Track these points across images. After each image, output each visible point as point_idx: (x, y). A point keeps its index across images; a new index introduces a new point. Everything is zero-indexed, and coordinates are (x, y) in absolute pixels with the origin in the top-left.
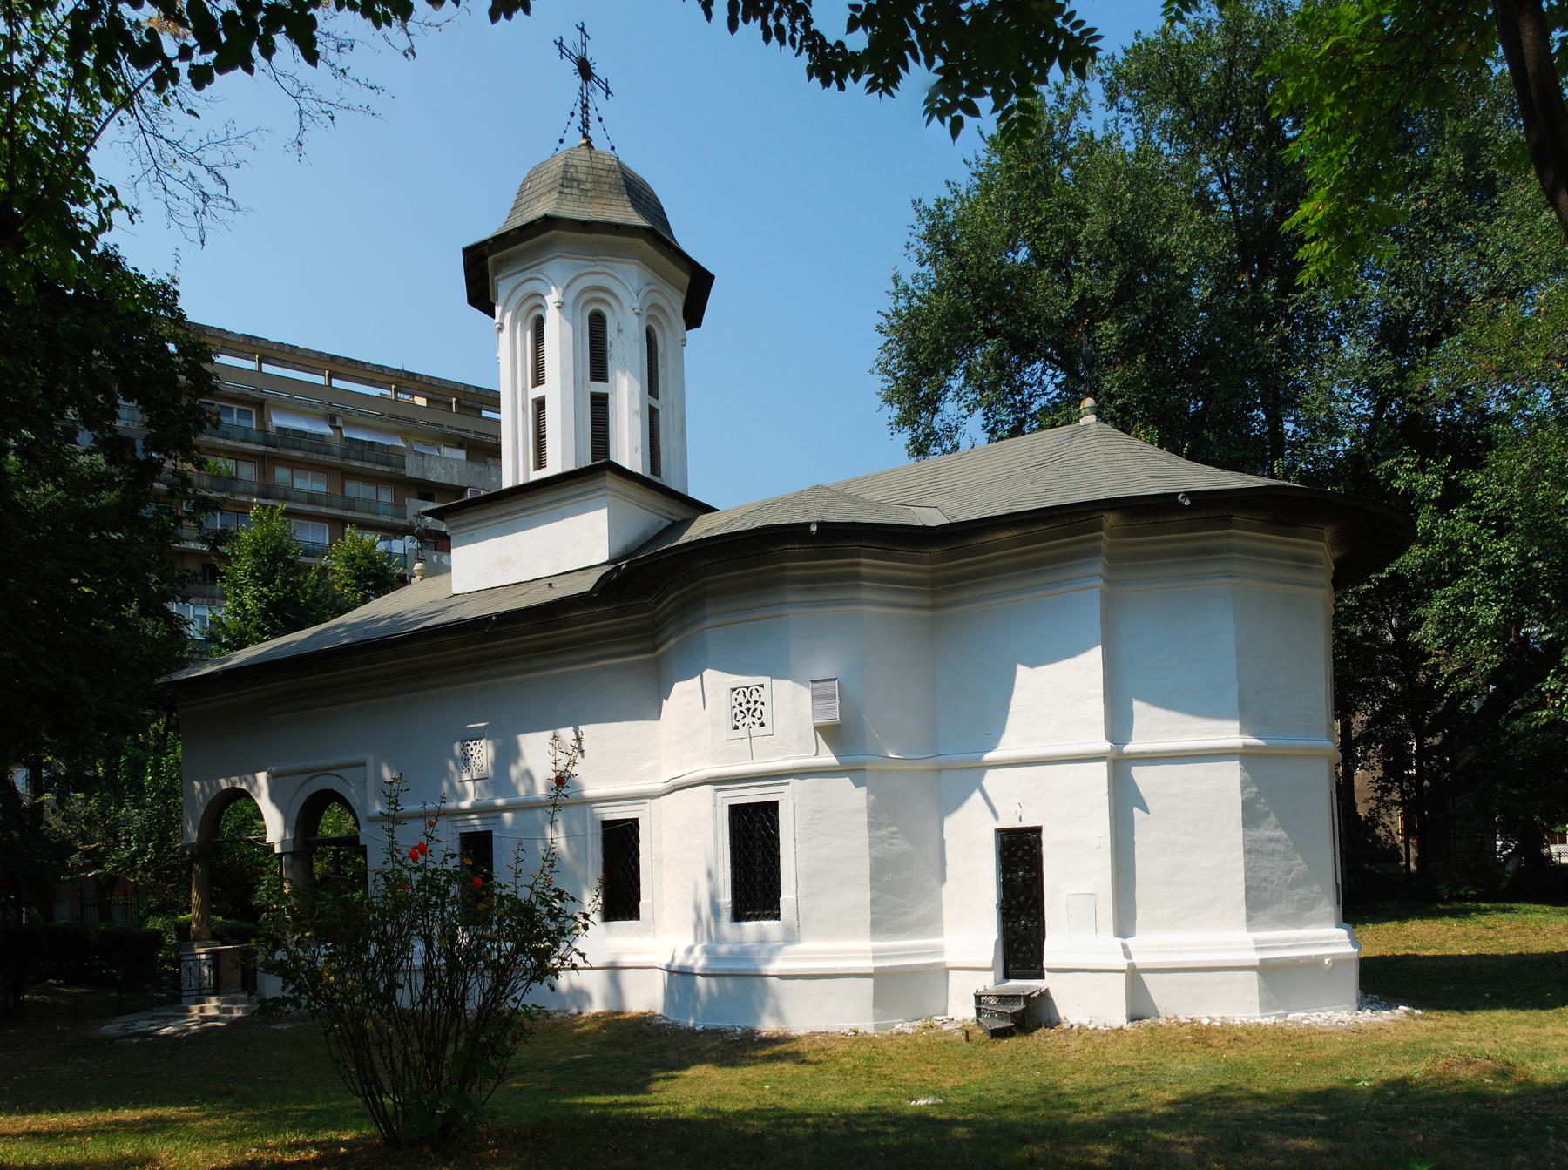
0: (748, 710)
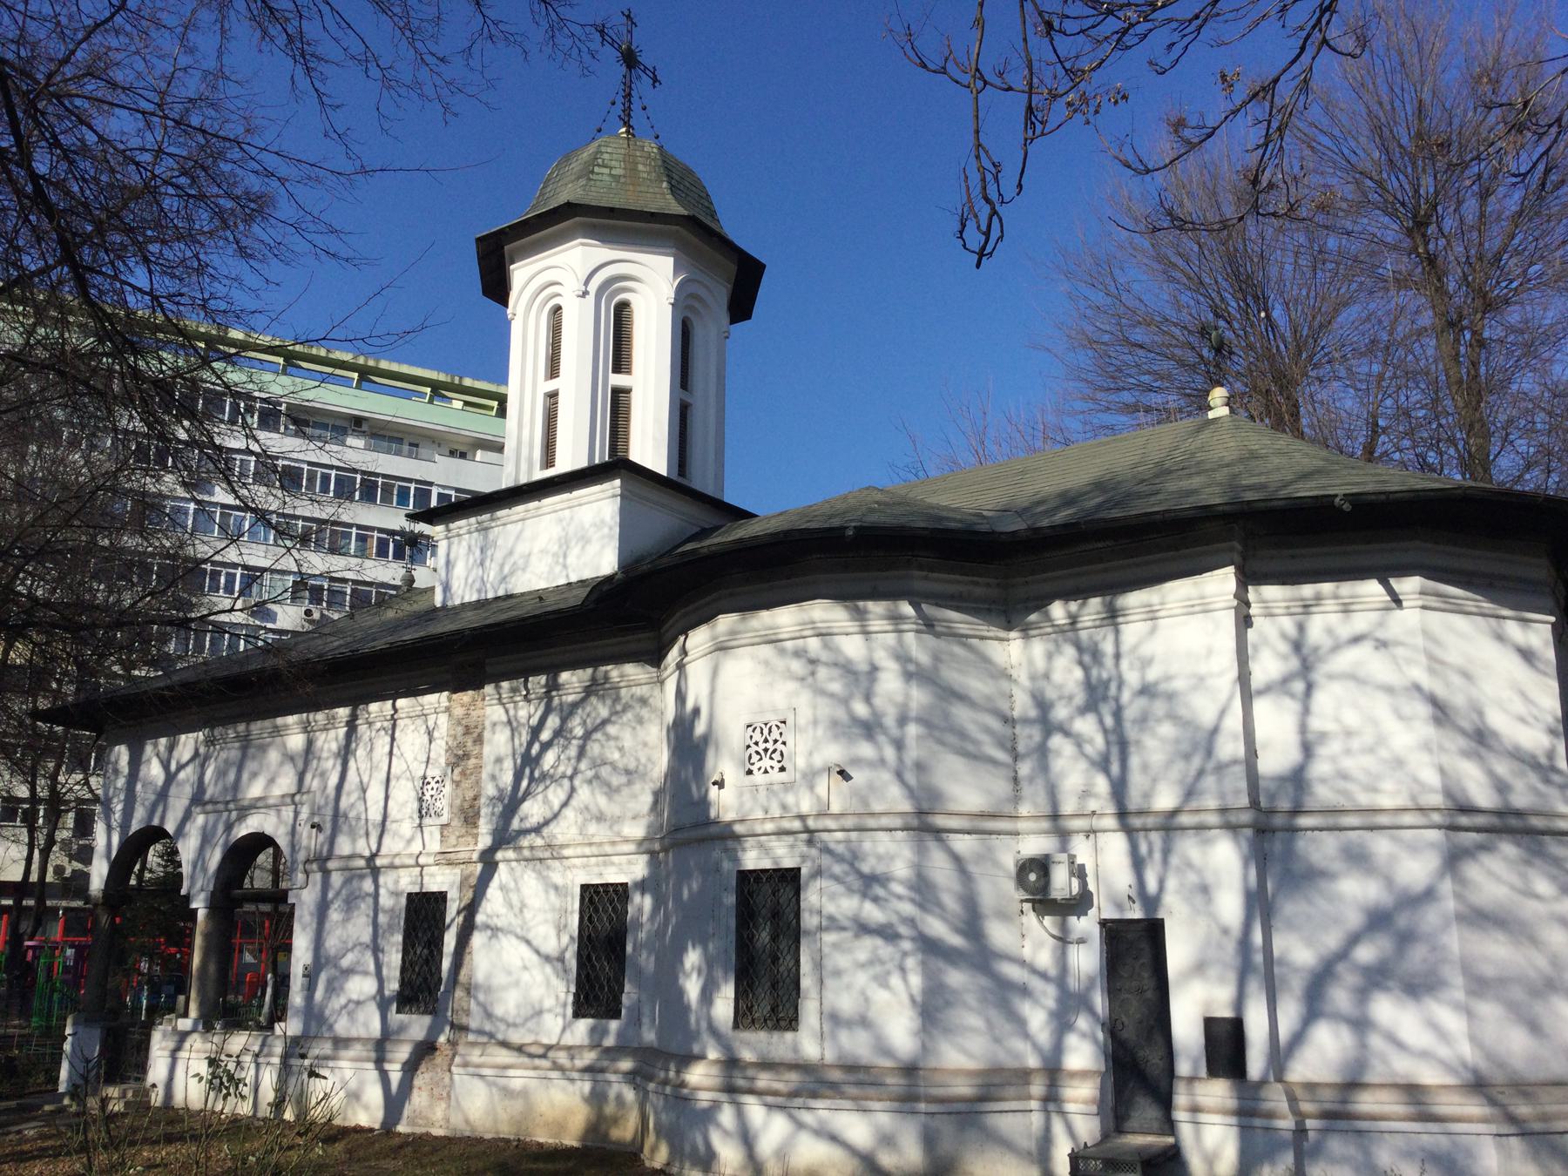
0: (766, 750)
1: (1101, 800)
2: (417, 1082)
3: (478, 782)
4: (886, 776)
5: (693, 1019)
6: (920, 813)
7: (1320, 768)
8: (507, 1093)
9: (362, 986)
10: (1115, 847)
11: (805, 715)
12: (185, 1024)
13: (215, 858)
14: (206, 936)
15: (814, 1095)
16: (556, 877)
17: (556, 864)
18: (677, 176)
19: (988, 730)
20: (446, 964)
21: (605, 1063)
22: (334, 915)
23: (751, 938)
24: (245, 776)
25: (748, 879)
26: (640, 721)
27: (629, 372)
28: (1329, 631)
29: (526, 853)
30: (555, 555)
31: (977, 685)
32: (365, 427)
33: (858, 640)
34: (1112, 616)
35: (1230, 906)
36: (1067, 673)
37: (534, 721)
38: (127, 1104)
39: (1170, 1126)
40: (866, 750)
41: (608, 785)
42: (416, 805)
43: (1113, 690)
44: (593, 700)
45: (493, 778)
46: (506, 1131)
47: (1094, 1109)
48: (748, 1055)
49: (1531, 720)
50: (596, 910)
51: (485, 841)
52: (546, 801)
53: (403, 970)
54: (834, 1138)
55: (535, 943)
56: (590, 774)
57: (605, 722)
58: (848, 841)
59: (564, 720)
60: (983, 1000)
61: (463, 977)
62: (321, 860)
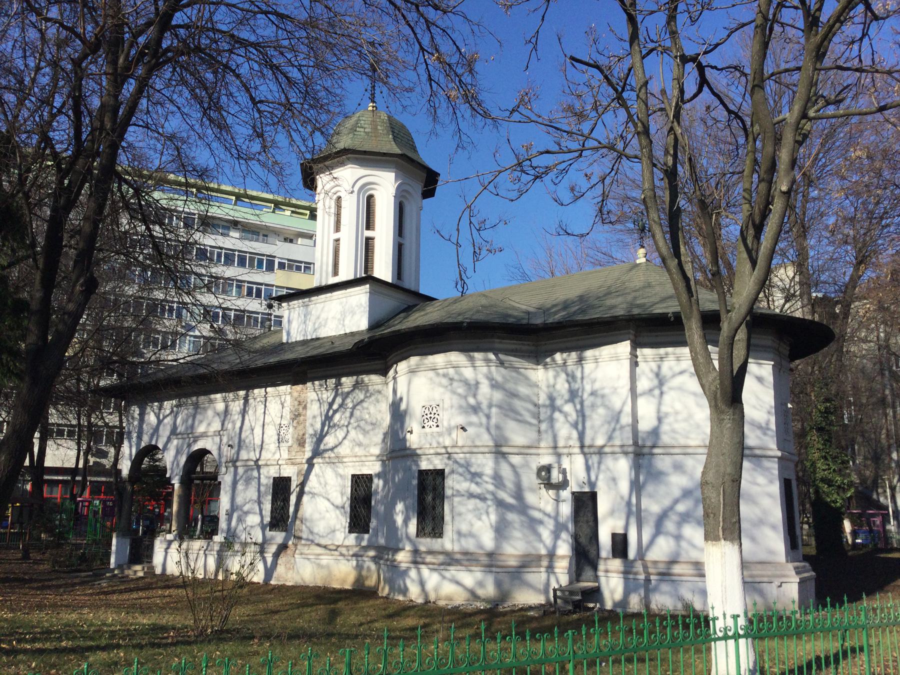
1: (574, 442)
2: (279, 562)
3: (305, 427)
4: (483, 430)
5: (399, 533)
6: (497, 446)
7: (665, 428)
8: (320, 566)
9: (253, 520)
10: (579, 460)
11: (447, 404)
12: (170, 537)
13: (183, 459)
14: (180, 497)
15: (449, 564)
16: (341, 471)
17: (340, 465)
18: (399, 132)
19: (528, 410)
20: (292, 509)
21: (362, 553)
22: (240, 487)
23: (424, 499)
24: (196, 423)
25: (423, 474)
26: (378, 401)
27: (373, 230)
28: (671, 368)
29: (327, 460)
30: (339, 320)
31: (523, 390)
32: (239, 227)
33: (471, 369)
34: (581, 360)
35: (624, 486)
36: (562, 386)
37: (330, 400)
38: (145, 573)
39: (596, 578)
40: (474, 419)
41: (364, 430)
42: (276, 437)
43: (580, 394)
44: (357, 391)
45: (312, 425)
46: (320, 583)
47: (566, 571)
48: (423, 548)
49: (758, 407)
50: (358, 486)
51: (308, 454)
52: (336, 436)
53: (272, 512)
54: (458, 583)
55: (332, 500)
56: (355, 424)
57: (362, 401)
58: (465, 458)
59: (343, 400)
60: (522, 526)
61: (300, 514)
62: (234, 462)
